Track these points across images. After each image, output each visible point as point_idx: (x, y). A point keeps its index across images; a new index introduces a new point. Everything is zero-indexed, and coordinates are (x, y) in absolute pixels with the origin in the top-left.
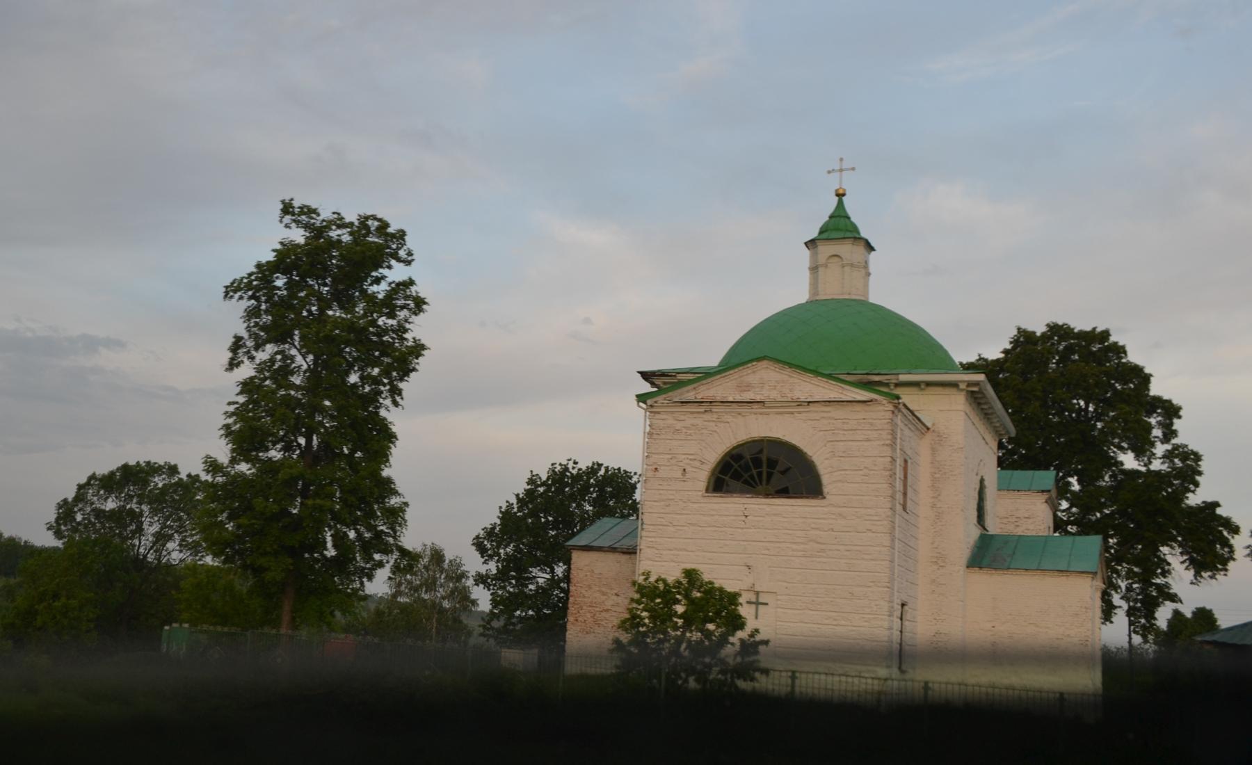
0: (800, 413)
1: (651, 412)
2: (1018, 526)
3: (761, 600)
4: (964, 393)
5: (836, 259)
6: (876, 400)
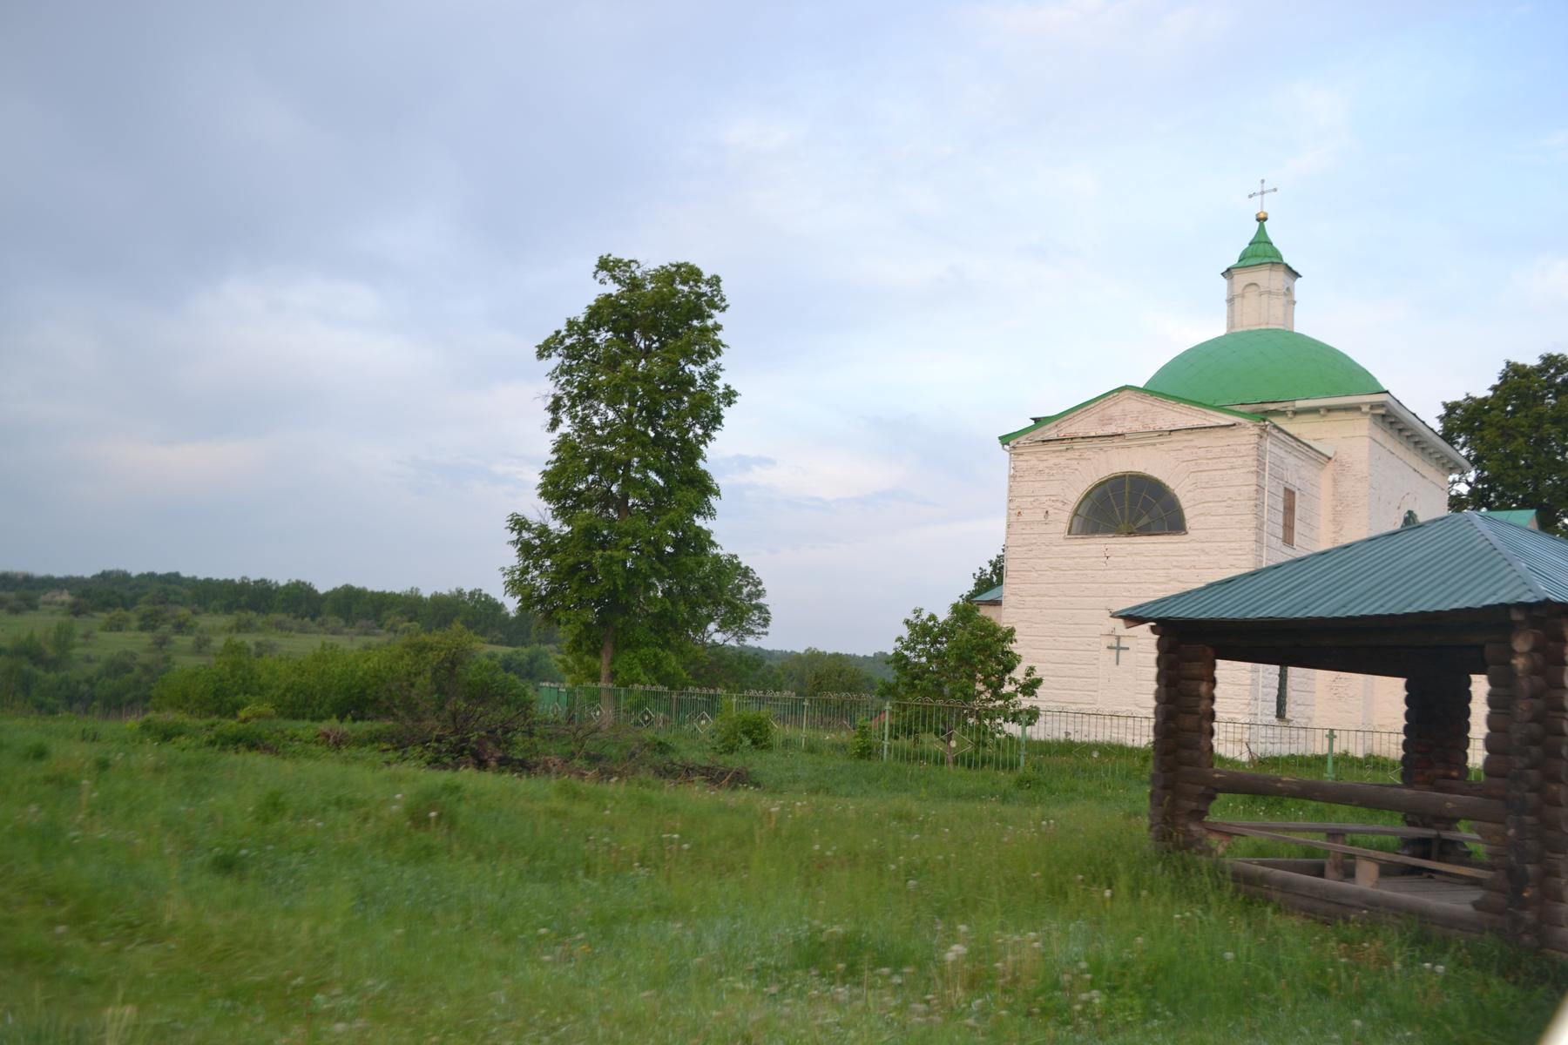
0: (1162, 443)
1: (1015, 454)
3: (1122, 645)
4: (1369, 417)
5: (1254, 288)
6: (1240, 424)
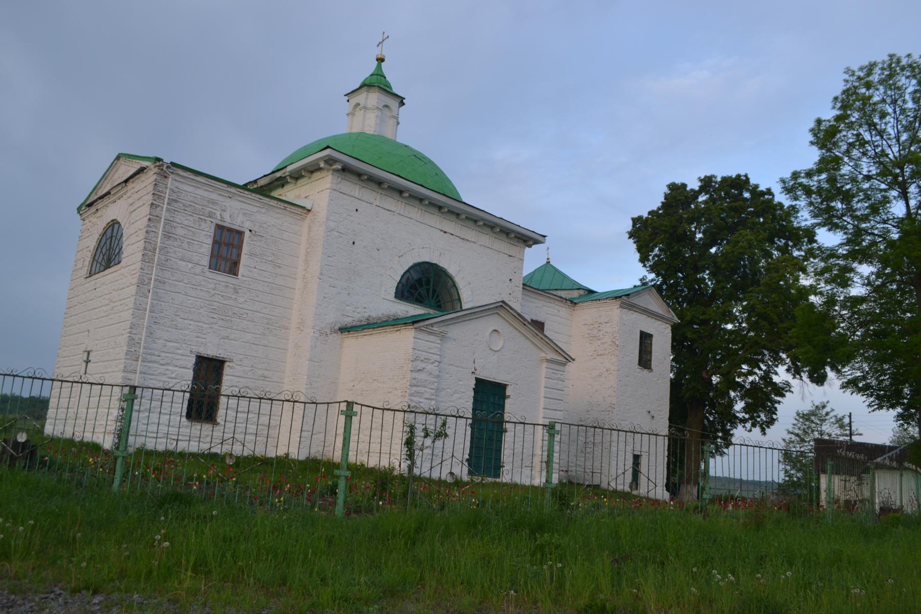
2: (600, 330)
